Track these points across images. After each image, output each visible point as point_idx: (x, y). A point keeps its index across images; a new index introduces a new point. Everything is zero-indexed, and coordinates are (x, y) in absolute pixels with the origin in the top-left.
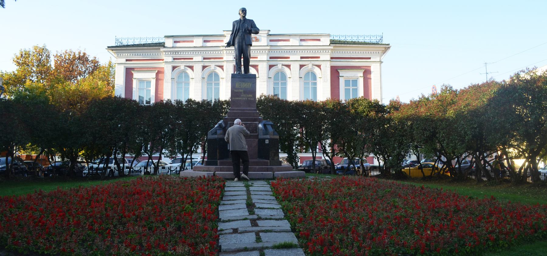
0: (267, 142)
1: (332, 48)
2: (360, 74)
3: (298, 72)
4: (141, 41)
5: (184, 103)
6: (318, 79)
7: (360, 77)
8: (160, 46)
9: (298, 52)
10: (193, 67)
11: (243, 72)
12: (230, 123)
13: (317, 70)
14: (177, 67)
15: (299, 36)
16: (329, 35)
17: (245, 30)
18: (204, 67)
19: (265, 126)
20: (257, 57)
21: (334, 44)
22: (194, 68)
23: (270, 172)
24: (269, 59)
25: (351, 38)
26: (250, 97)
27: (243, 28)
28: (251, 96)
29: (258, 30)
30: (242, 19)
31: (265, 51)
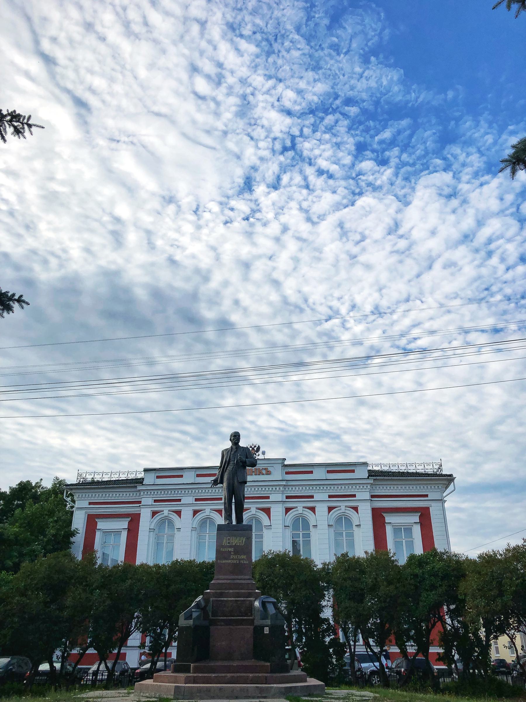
0: (266, 630)
2: (416, 518)
4: (112, 476)
7: (415, 523)
8: (137, 483)
11: (234, 522)
12: (213, 600)
16: (365, 464)
18: (195, 512)
19: (263, 604)
20: (141, 502)
21: (373, 476)
22: (316, 509)
24: (285, 500)
25: (396, 468)
26: (243, 559)
27: (235, 459)
28: (244, 557)
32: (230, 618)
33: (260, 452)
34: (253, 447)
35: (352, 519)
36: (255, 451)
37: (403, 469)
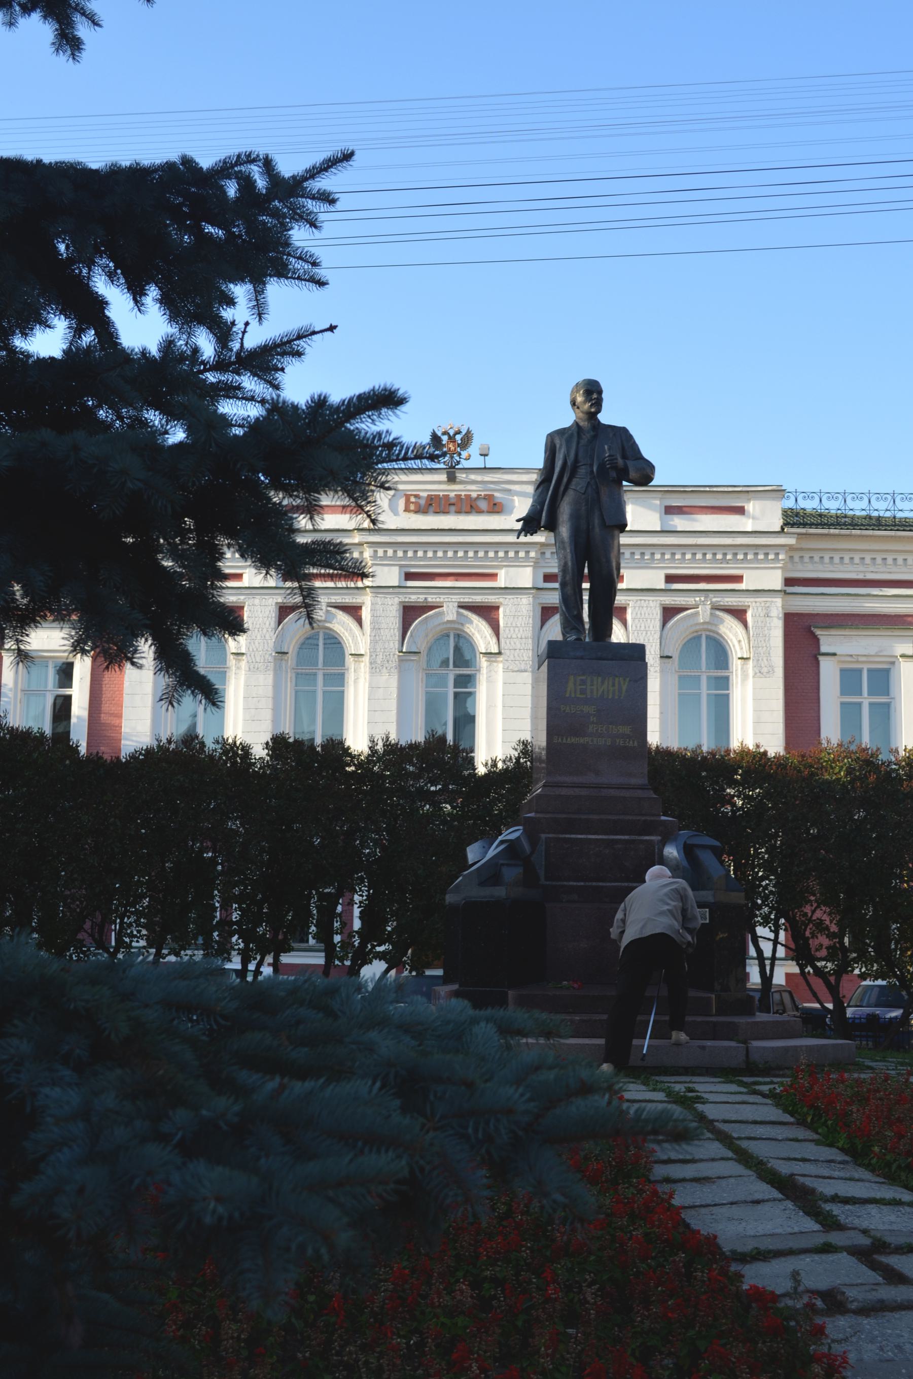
1: (792, 541)
3: (657, 636)
5: (259, 752)
6: (736, 665)
7: (903, 656)
9: (658, 556)
10: (243, 608)
12: (546, 838)
13: (730, 630)
14: (432, 608)
15: (659, 495)
16: (778, 492)
17: (602, 466)
23: (733, 1044)
25: (864, 504)
28: (627, 730)
29: (648, 470)
30: (584, 424)
31: (527, 552)
32: (594, 884)
33: (474, 449)
34: (452, 433)
35: (727, 642)
36: (459, 445)
37: (832, 506)
